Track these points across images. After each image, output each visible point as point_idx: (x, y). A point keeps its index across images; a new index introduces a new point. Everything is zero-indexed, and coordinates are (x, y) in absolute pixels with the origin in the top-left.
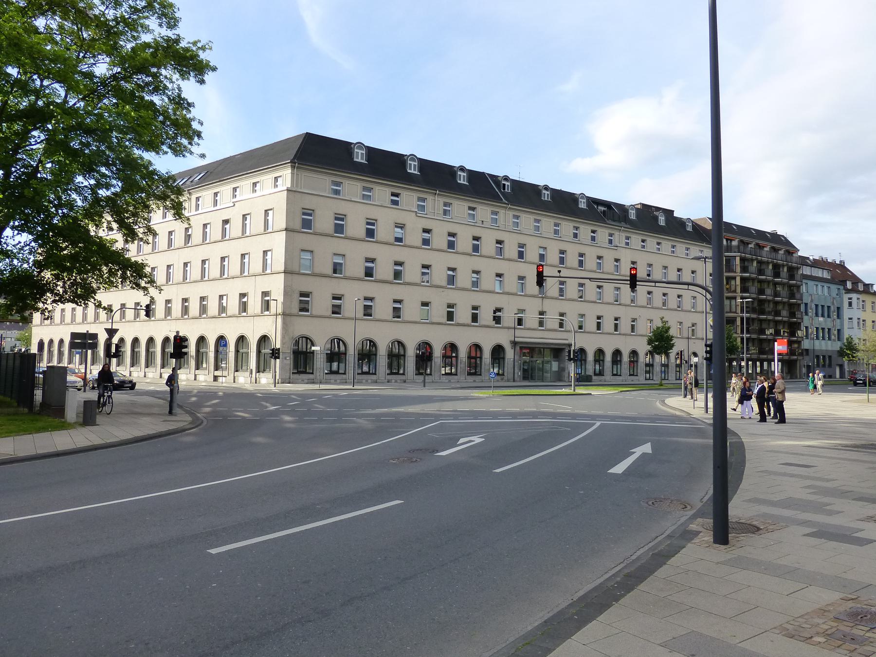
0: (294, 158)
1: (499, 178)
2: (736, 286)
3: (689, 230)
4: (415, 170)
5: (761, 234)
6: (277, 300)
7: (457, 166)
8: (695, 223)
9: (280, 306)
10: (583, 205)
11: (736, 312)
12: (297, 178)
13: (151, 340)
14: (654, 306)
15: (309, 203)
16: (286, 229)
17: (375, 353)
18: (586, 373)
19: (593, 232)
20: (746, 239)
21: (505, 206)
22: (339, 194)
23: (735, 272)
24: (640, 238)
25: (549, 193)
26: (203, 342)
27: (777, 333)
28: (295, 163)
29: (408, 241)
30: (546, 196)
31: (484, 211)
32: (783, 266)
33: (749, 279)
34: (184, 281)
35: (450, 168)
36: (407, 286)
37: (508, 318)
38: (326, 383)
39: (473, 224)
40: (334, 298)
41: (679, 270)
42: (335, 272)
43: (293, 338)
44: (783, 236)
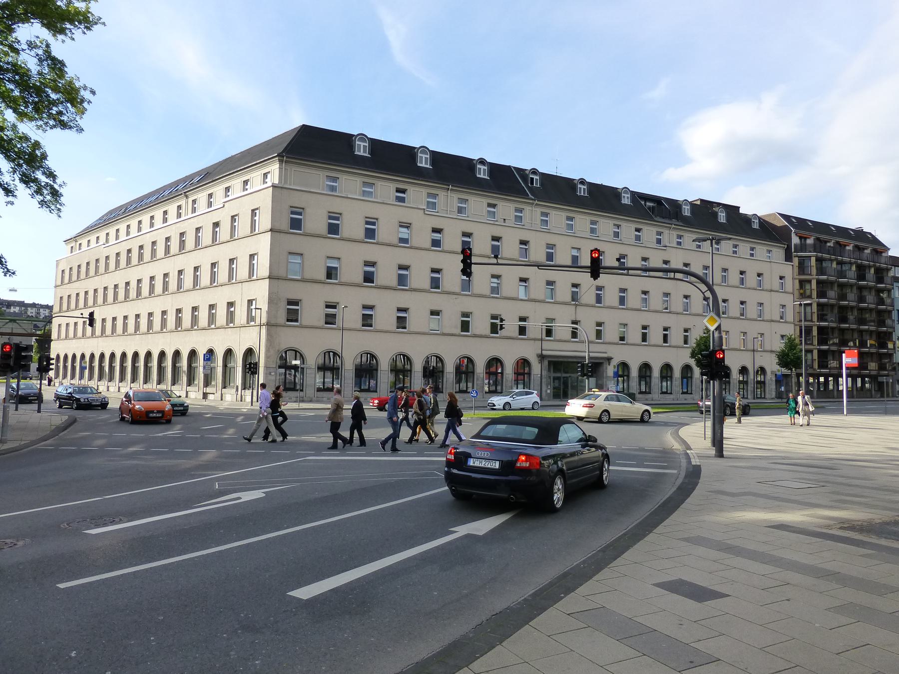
0: (283, 151)
1: (526, 172)
2: (811, 290)
3: (755, 227)
4: (484, 174)
5: (843, 232)
6: (261, 309)
7: (476, 158)
8: (764, 220)
9: (264, 315)
10: (626, 200)
11: (811, 321)
12: (286, 175)
15: (298, 200)
16: (271, 230)
17: (441, 369)
18: (629, 391)
19: (638, 230)
20: (823, 237)
21: (531, 201)
22: (336, 191)
23: (810, 275)
24: (634, 226)
25: (585, 187)
26: (251, 355)
27: (844, 343)
28: (283, 157)
29: (414, 242)
30: (582, 190)
31: (506, 208)
32: (870, 267)
33: (848, 285)
34: (178, 290)
35: (350, 136)
36: (413, 292)
37: (535, 327)
38: (318, 401)
39: (521, 227)
40: (327, 306)
41: (742, 273)
43: (278, 351)
44: (870, 233)
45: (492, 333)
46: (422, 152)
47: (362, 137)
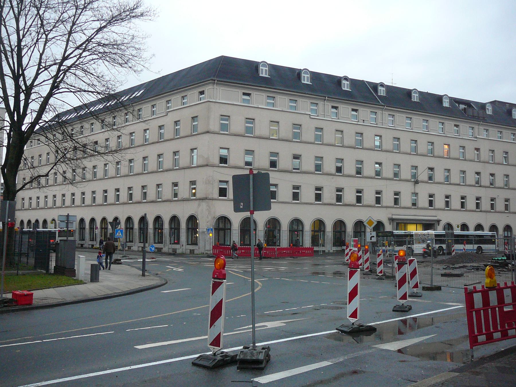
4: (308, 81)
13: (93, 220)
14: (467, 184)
21: (382, 107)
30: (382, 92)
42: (377, 175)
43: (214, 217)
45: (395, 204)
46: (263, 66)
47: (264, 63)
